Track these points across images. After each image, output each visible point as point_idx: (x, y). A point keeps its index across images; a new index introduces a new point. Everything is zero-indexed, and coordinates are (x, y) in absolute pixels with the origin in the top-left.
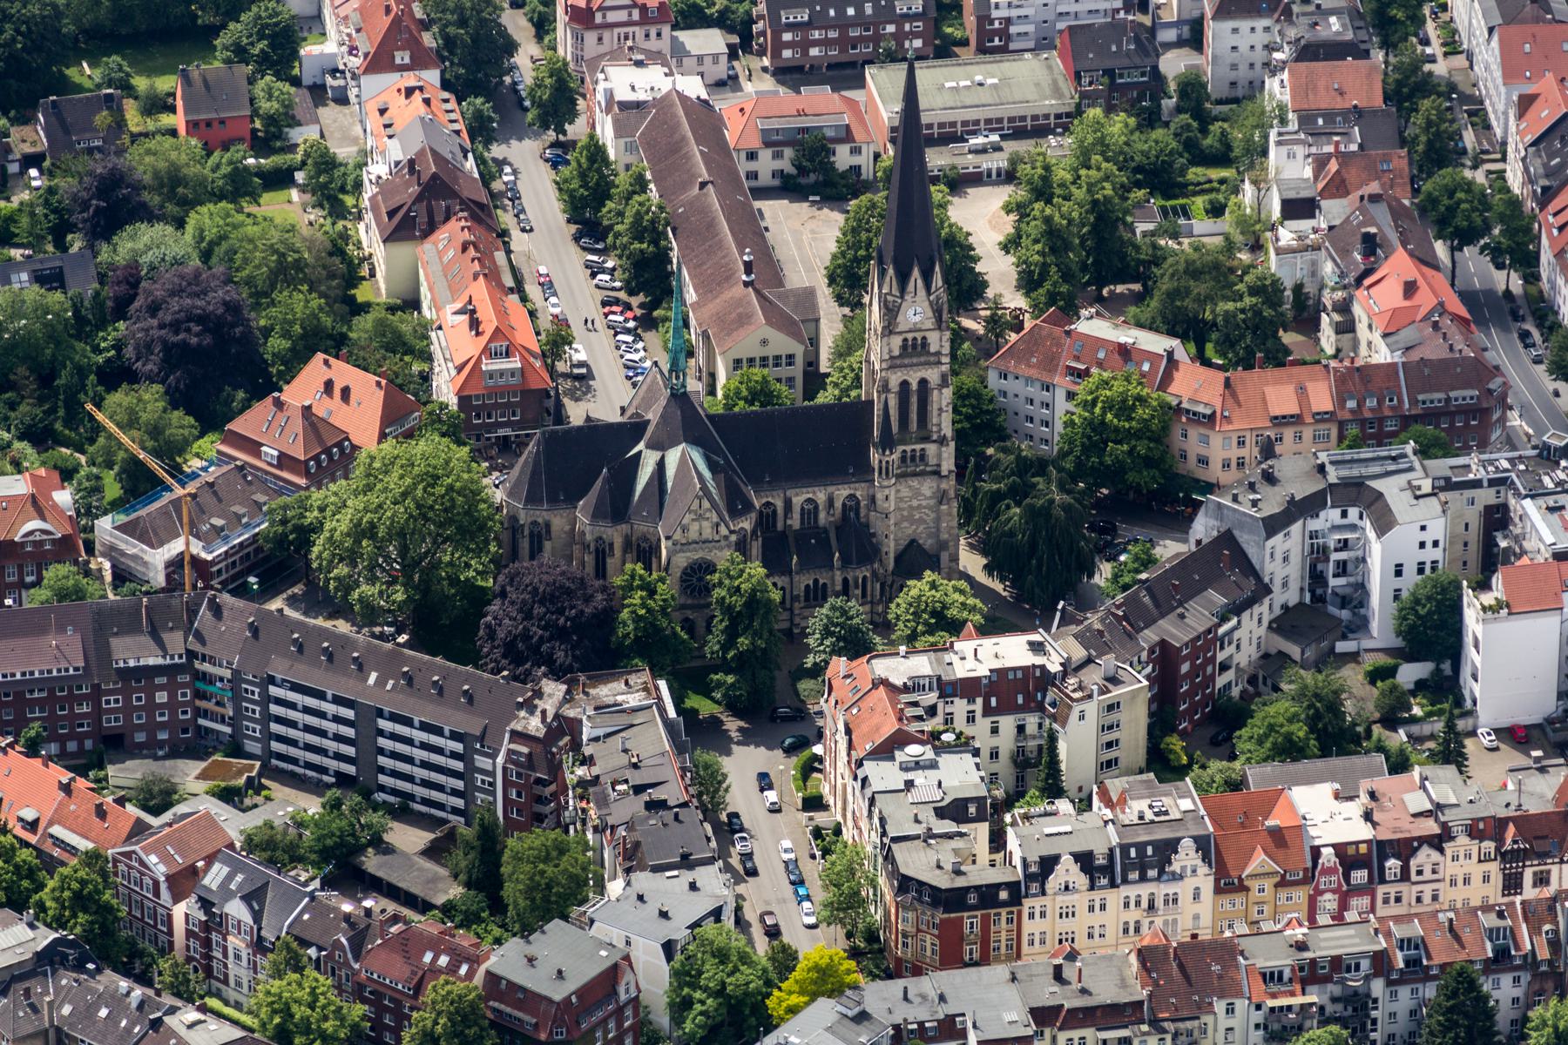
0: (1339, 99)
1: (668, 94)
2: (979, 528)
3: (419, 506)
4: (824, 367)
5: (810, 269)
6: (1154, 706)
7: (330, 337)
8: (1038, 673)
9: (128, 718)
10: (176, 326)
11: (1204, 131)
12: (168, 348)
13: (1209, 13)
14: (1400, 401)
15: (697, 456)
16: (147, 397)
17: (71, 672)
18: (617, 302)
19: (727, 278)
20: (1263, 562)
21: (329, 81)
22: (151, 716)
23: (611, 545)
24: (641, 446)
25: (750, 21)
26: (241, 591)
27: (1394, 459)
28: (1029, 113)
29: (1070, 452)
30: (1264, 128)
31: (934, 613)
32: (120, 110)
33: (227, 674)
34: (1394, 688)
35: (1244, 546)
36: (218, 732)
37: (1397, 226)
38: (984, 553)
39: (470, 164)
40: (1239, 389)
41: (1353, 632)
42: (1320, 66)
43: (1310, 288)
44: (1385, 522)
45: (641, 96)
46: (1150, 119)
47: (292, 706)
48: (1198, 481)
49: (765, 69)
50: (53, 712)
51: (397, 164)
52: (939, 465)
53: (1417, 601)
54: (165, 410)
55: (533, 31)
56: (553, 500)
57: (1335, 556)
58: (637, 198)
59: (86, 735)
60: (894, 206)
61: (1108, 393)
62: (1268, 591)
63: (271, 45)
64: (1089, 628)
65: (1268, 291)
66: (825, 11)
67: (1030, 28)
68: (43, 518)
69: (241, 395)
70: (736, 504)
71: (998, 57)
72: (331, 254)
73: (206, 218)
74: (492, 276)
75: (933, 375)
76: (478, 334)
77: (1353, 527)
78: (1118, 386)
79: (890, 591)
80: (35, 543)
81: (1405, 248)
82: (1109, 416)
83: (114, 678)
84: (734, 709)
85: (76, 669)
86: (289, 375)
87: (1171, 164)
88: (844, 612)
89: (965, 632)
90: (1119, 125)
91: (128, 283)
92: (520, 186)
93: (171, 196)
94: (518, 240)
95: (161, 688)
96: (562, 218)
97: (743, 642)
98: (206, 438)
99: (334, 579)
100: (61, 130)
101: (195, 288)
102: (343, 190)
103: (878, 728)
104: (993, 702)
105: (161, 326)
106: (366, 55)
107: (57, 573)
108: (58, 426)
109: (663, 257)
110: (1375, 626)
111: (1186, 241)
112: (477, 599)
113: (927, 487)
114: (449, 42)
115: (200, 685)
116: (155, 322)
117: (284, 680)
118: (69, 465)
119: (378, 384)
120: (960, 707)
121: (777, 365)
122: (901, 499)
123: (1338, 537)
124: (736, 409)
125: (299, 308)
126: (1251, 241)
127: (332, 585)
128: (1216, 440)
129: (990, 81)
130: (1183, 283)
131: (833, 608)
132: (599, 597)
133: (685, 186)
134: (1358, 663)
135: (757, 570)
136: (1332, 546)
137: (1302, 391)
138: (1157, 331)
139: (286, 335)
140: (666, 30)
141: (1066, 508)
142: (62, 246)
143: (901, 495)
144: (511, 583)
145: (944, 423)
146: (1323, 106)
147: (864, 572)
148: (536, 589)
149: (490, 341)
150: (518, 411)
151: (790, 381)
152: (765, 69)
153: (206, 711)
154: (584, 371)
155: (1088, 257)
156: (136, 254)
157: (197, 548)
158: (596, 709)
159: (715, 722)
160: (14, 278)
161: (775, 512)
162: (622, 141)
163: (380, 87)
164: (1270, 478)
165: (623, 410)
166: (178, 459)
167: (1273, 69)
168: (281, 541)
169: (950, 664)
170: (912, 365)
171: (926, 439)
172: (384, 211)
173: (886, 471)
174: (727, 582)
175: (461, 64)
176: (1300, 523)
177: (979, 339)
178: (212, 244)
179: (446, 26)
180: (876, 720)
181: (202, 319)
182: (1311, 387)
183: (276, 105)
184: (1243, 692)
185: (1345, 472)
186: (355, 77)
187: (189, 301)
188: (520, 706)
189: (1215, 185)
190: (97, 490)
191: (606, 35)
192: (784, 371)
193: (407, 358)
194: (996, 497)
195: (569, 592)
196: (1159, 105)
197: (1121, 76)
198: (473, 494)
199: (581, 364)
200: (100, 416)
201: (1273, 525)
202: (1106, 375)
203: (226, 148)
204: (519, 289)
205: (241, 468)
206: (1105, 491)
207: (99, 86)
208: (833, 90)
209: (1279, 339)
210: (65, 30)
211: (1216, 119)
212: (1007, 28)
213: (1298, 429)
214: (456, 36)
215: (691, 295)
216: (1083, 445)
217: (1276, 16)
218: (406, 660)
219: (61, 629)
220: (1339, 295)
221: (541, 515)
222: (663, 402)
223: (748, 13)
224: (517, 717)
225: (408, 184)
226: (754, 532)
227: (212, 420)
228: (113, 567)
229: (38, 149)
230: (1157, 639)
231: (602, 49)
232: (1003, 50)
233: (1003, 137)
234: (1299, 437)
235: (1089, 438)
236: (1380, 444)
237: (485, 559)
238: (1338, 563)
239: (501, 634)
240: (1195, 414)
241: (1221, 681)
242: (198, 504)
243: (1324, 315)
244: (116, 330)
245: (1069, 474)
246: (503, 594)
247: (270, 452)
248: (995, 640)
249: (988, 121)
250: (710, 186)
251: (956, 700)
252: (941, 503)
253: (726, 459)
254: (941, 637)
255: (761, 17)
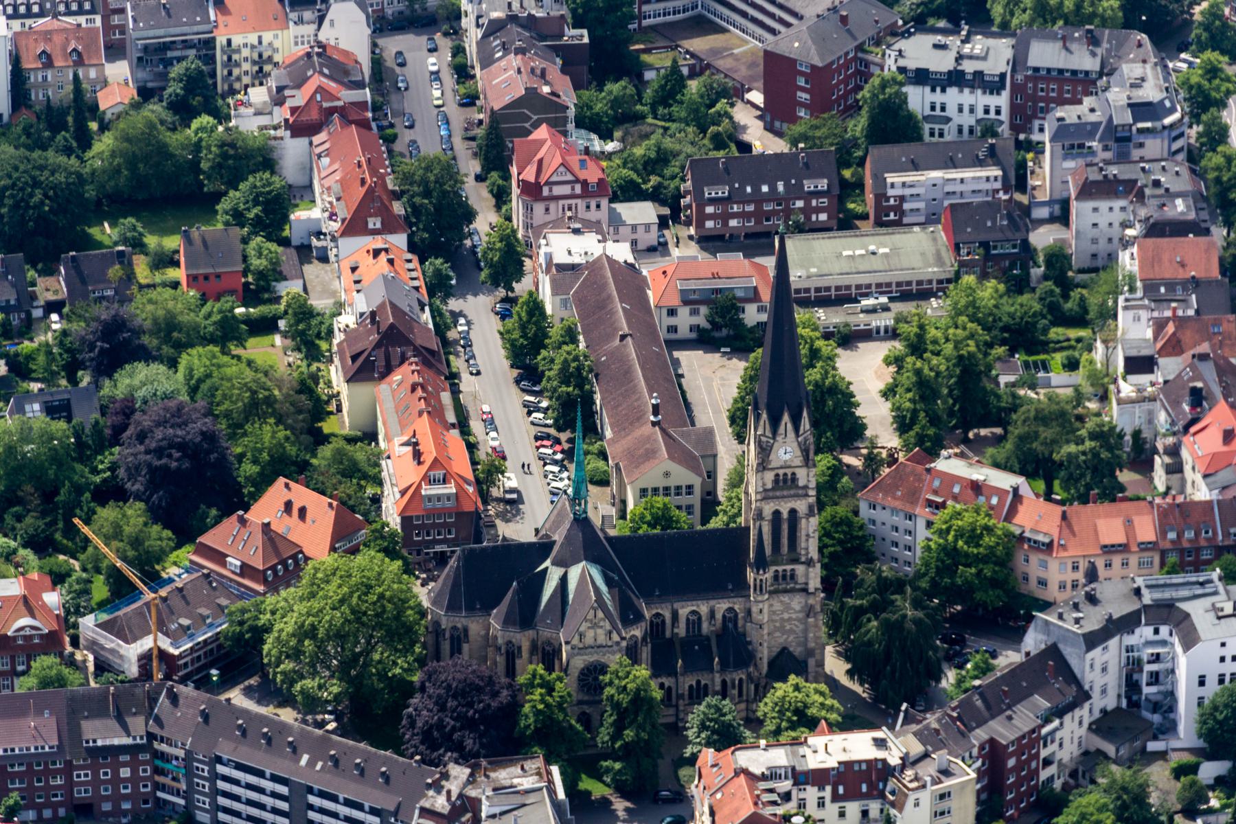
0: (1181, 270)
1: (599, 258)
2: (846, 638)
3: (353, 612)
4: (721, 495)
5: (717, 412)
6: (984, 796)
7: (295, 463)
8: (880, 766)
9: (96, 790)
10: (159, 452)
11: (1066, 297)
12: (152, 470)
13: (1073, 196)
14: (1215, 533)
15: (595, 572)
16: (130, 512)
17: (47, 749)
18: (548, 437)
19: (639, 418)
20: (1083, 672)
21: (315, 242)
22: (116, 789)
23: (520, 648)
24: (547, 563)
25: (679, 196)
26: (202, 683)
27: (1202, 584)
28: (915, 279)
29: (925, 575)
30: (1116, 293)
31: (797, 712)
32: (130, 264)
33: (181, 753)
34: (1193, 783)
35: (1068, 658)
36: (174, 804)
37: (1221, 381)
38: (848, 659)
39: (426, 316)
40: (1074, 521)
41: (1163, 733)
42: (1165, 242)
43: (1146, 434)
44: (1190, 639)
45: (576, 260)
46: (1019, 285)
47: (236, 782)
48: (1037, 600)
49: (691, 238)
50: (31, 783)
51: (362, 315)
52: (807, 584)
53: (1215, 708)
54: (145, 524)
55: (493, 201)
56: (471, 609)
57: (1148, 668)
58: (565, 348)
59: (60, 804)
60: (768, 361)
61: (960, 523)
62: (1087, 696)
63: (263, 211)
64: (927, 727)
65: (1107, 436)
66: (743, 188)
67: (921, 205)
68: (33, 616)
69: (214, 512)
70: (629, 615)
71: (890, 230)
72: (299, 392)
73: (195, 359)
74: (436, 413)
75: (801, 506)
76: (419, 463)
77: (1164, 643)
78: (968, 518)
79: (761, 691)
80: (25, 638)
81: (1227, 401)
82: (960, 543)
83: (84, 755)
84: (623, 791)
85: (51, 748)
86: (255, 497)
87: (1034, 324)
88: (718, 710)
89: (819, 728)
90: (990, 290)
91: (125, 414)
92: (472, 335)
93: (167, 339)
94: (467, 384)
95: (125, 765)
96: (507, 364)
97: (629, 734)
98: (183, 549)
99: (281, 673)
100: (80, 281)
101: (179, 420)
102: (318, 336)
103: (736, 811)
104: (841, 790)
105: (147, 452)
106: (343, 220)
107: (45, 663)
108: (58, 536)
109: (588, 400)
110: (1181, 728)
111: (1042, 391)
112: (404, 690)
113: (797, 602)
114: (416, 210)
115: (158, 763)
116: (142, 448)
117: (230, 760)
118: (63, 570)
119: (330, 505)
120: (811, 794)
121: (678, 494)
122: (774, 612)
123: (1150, 651)
124: (641, 532)
125: (267, 438)
126: (1100, 392)
127: (279, 678)
128: (1053, 565)
129: (882, 251)
130: (1033, 428)
131: (709, 706)
132: (505, 693)
133: (609, 337)
134: (1166, 760)
135: (642, 672)
136: (1145, 659)
137: (1129, 524)
138: (1014, 472)
139: (255, 461)
140: (604, 202)
141: (917, 622)
142: (73, 381)
143: (774, 608)
144: (429, 679)
145: (810, 546)
146: (1167, 276)
147: (740, 675)
148: (449, 686)
149: (430, 469)
150: (453, 531)
151: (689, 510)
152: (691, 238)
153: (164, 785)
154: (514, 496)
155: (954, 405)
156: (133, 389)
157: (165, 644)
158: (494, 790)
159: (605, 803)
160: (27, 408)
161: (663, 622)
162: (558, 298)
163: (354, 248)
164: (1092, 599)
165: (537, 531)
166: (157, 567)
167: (1126, 244)
168: (238, 639)
169: (804, 756)
170: (783, 497)
171: (796, 561)
172: (348, 355)
173: (760, 589)
174: (616, 682)
175: (424, 230)
176: (1116, 640)
177: (859, 473)
178: (200, 381)
179: (413, 196)
180: (736, 804)
181: (182, 447)
182: (1137, 520)
183: (264, 262)
184: (1065, 785)
185: (1158, 595)
186: (334, 239)
187: (171, 431)
188: (429, 786)
189: (1073, 343)
190: (86, 592)
191: (552, 206)
192: (684, 500)
193: (363, 483)
194: (859, 612)
195: (479, 690)
196: (1028, 274)
197: (995, 248)
198: (402, 601)
199: (512, 491)
200: (86, 530)
201: (1093, 640)
202: (958, 507)
203: (218, 299)
204: (463, 425)
205: (207, 576)
206: (959, 608)
207: (116, 244)
208: (745, 256)
209: (1116, 478)
210: (87, 195)
211: (1078, 286)
212: (901, 205)
213: (1125, 556)
214: (421, 205)
215: (608, 433)
216: (937, 567)
217: (1131, 197)
218: (335, 745)
219: (40, 713)
220: (1171, 440)
221: (461, 621)
222: (567, 525)
223: (678, 188)
224: (425, 796)
225: (369, 333)
226: (644, 639)
227: (186, 533)
228: (96, 658)
229: (59, 297)
230: (986, 737)
231: (548, 218)
232: (898, 223)
233: (891, 299)
234: (1125, 564)
235: (943, 562)
236: (1197, 571)
237: (410, 658)
238: (1151, 674)
239: (419, 724)
240: (1035, 542)
241: (1044, 775)
242: (168, 606)
243: (1157, 458)
244: (112, 454)
245: (925, 592)
246: (423, 689)
247: (234, 562)
248: (844, 736)
249: (879, 285)
250: (629, 339)
251: (808, 788)
252: (808, 616)
253: (620, 574)
254: (802, 732)
255: (687, 192)
